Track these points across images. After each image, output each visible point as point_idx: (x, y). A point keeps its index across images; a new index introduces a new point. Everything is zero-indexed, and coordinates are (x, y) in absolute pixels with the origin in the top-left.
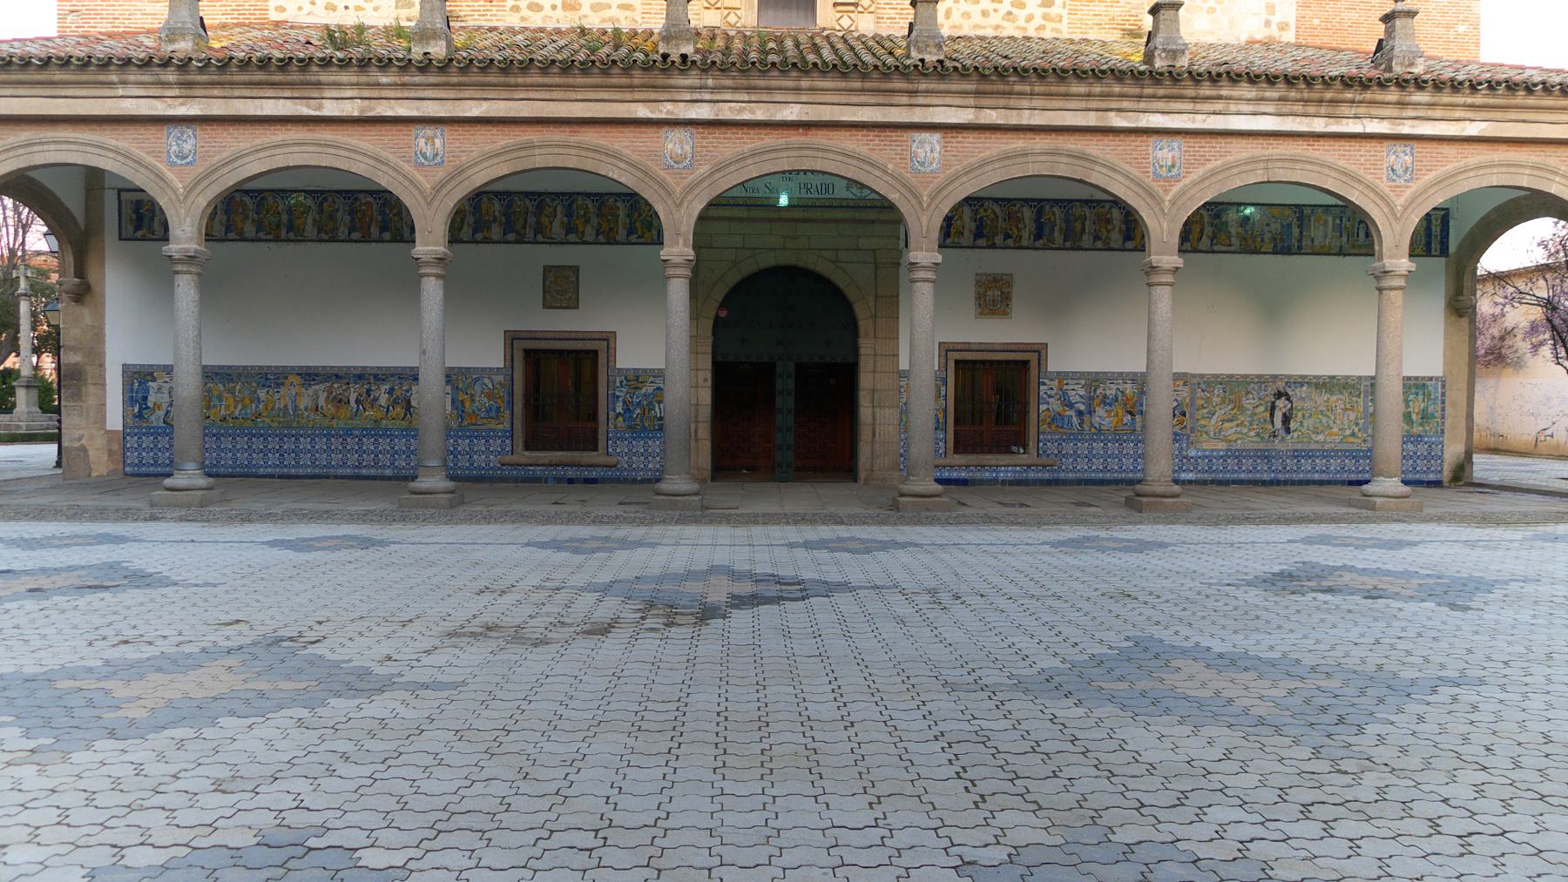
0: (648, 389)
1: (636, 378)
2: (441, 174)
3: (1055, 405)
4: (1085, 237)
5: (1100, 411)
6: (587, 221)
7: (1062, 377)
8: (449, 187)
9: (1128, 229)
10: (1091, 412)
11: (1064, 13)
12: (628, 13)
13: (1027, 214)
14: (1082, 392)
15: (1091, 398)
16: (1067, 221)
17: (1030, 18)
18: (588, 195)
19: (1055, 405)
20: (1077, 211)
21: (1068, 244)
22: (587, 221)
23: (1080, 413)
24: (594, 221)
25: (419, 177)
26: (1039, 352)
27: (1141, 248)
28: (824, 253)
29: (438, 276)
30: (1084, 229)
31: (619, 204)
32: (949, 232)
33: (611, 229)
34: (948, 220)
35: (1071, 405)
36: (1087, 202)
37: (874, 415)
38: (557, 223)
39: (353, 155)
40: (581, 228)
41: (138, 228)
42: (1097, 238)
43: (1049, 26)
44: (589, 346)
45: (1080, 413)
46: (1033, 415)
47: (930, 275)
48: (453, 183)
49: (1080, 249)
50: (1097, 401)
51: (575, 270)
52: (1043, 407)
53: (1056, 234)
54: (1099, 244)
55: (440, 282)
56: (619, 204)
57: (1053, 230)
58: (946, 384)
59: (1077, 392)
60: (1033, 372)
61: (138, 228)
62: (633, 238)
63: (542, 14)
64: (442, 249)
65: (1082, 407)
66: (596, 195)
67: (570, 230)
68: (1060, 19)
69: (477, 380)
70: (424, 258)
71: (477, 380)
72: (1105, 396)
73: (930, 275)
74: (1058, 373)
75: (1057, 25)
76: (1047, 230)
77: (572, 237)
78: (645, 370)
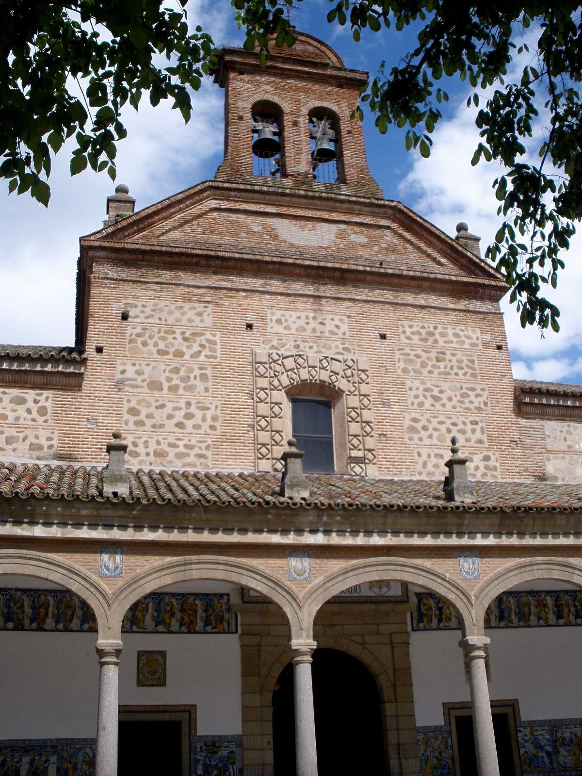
0: (224, 753)
1: (213, 744)
2: (120, 583)
3: (530, 748)
4: (532, 618)
5: (563, 751)
6: (173, 615)
7: (532, 724)
8: (126, 593)
9: (559, 611)
10: (557, 752)
11: (498, 465)
12: (202, 460)
13: (549, 601)
14: (548, 737)
15: (555, 741)
16: (519, 607)
17: (477, 468)
18: (197, 595)
19: (530, 748)
20: (524, 599)
21: (521, 623)
22: (173, 615)
23: (549, 754)
24: (178, 615)
25: (103, 584)
26: (513, 706)
27: (94, 630)
28: (353, 638)
29: (116, 664)
30: (530, 613)
31: (198, 602)
32: (133, 621)
33: (191, 622)
34: (134, 607)
35: (540, 747)
36: (566, 592)
37: (400, 765)
38: (148, 617)
39: (51, 567)
40: (167, 621)
41: (420, 620)
42: (539, 618)
43: (490, 473)
44: (174, 717)
45: (549, 754)
46: (516, 757)
47: (114, 659)
48: (129, 590)
49: (529, 626)
50: (559, 743)
51: (163, 654)
52: (522, 751)
53: (513, 616)
54: (542, 622)
55: (117, 668)
56: (198, 602)
57: (510, 614)
58: (451, 736)
59: (544, 736)
60: (511, 722)
61: (420, 620)
62: (209, 629)
63: (139, 458)
64: (120, 642)
65: (549, 749)
66: (179, 594)
67: (158, 621)
68: (495, 469)
69: (80, 749)
70: (107, 649)
71: (80, 749)
72: (564, 739)
73: (114, 659)
74: (529, 722)
75: (495, 473)
76: (506, 614)
77: (161, 628)
78: (220, 737)
